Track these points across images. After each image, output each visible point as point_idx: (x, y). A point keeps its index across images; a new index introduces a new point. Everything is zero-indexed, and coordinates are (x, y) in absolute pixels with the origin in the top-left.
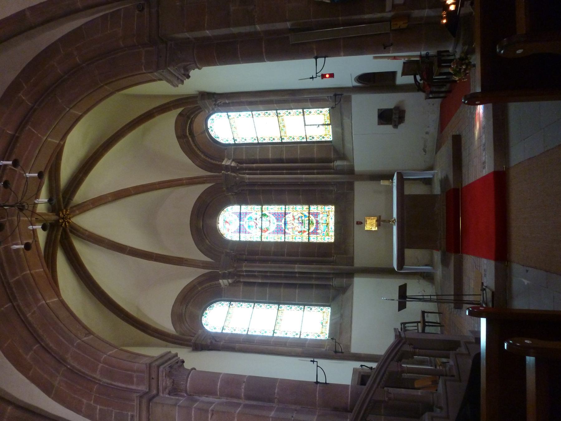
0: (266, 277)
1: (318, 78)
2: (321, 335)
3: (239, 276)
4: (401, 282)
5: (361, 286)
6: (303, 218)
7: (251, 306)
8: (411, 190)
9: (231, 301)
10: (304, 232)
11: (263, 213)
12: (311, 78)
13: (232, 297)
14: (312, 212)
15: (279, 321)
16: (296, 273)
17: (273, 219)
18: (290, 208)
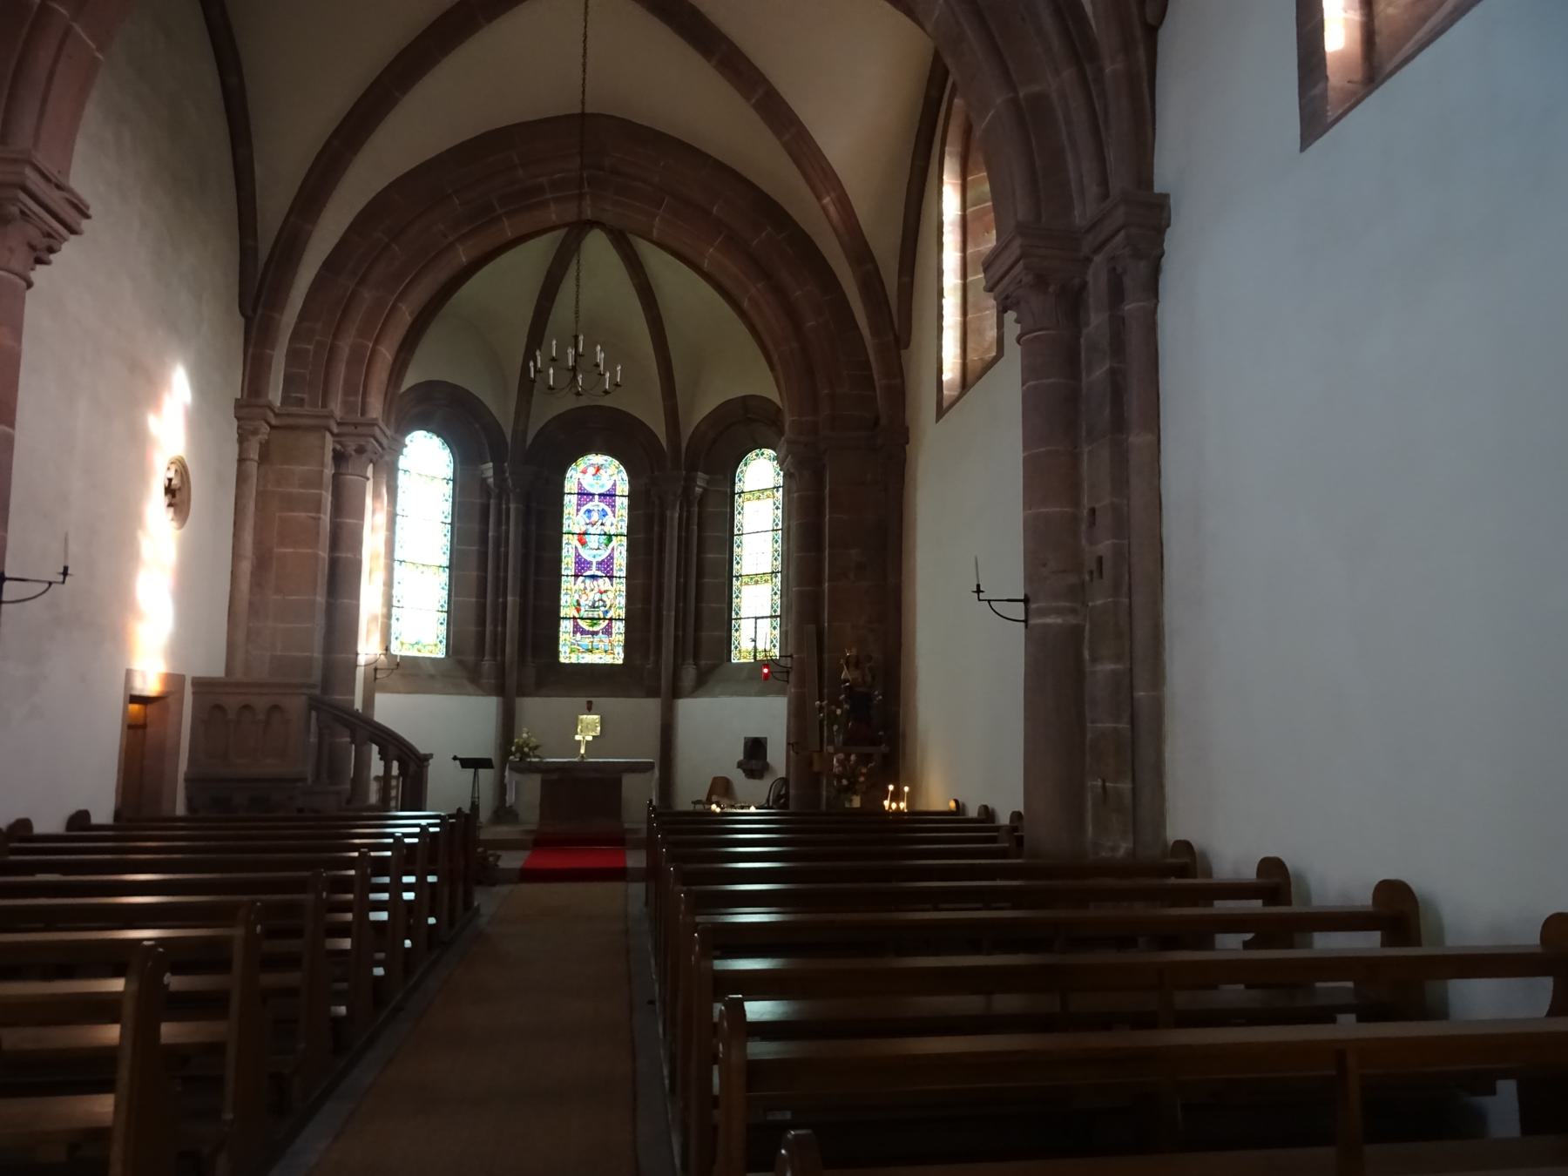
0: (497, 545)
3: (499, 497)
4: (495, 762)
5: (486, 708)
9: (454, 481)
10: (578, 611)
13: (462, 483)
17: (603, 555)
18: (621, 586)
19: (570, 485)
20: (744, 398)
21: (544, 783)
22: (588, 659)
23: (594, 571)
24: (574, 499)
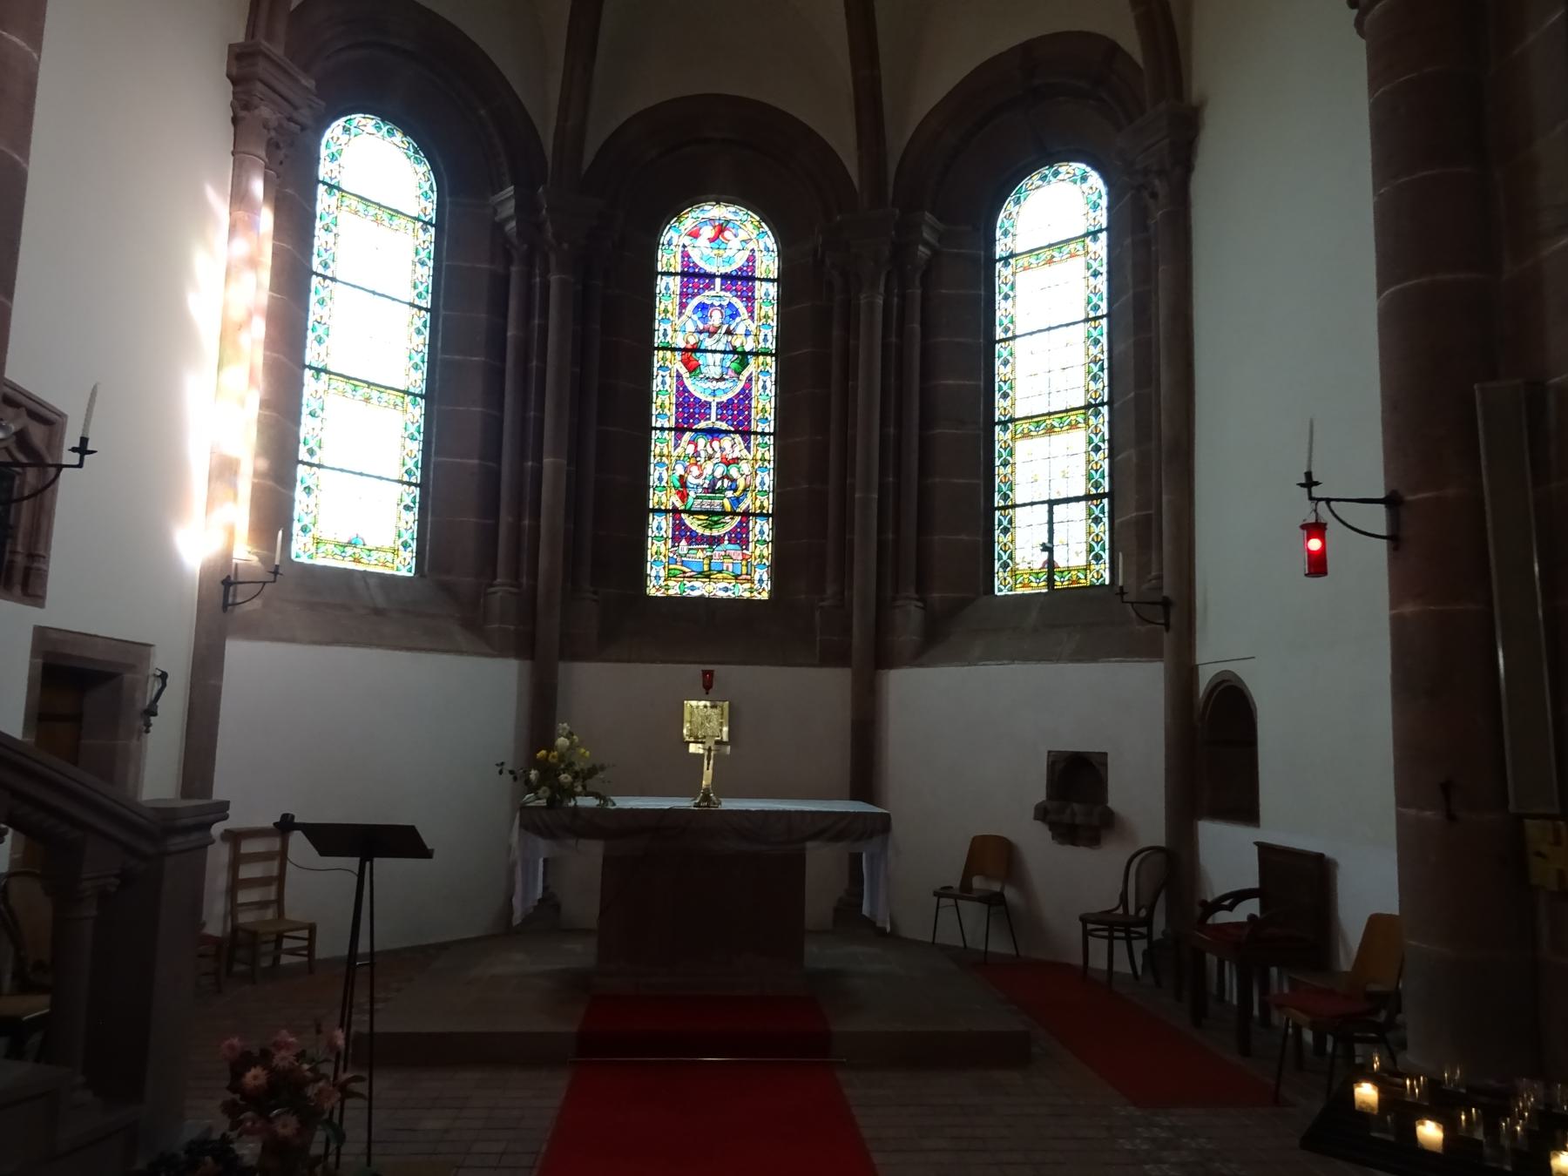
1: (1309, 505)
2: (308, 539)
6: (729, 494)
7: (419, 295)
8: (822, 865)
9: (438, 226)
10: (683, 496)
11: (752, 360)
12: (1309, 475)
14: (751, 524)
15: (363, 391)
16: (539, 459)
17: (729, 390)
19: (668, 259)
20: (1027, 48)
21: (609, 863)
22: (701, 589)
23: (713, 421)
24: (675, 283)
